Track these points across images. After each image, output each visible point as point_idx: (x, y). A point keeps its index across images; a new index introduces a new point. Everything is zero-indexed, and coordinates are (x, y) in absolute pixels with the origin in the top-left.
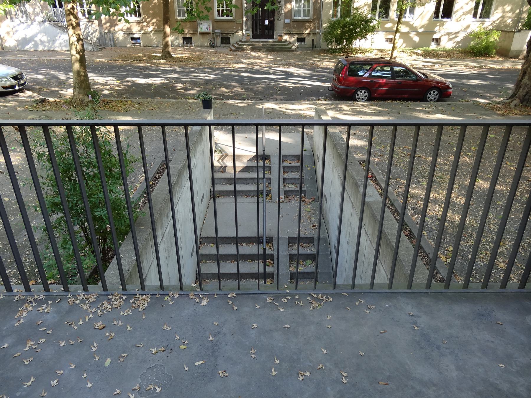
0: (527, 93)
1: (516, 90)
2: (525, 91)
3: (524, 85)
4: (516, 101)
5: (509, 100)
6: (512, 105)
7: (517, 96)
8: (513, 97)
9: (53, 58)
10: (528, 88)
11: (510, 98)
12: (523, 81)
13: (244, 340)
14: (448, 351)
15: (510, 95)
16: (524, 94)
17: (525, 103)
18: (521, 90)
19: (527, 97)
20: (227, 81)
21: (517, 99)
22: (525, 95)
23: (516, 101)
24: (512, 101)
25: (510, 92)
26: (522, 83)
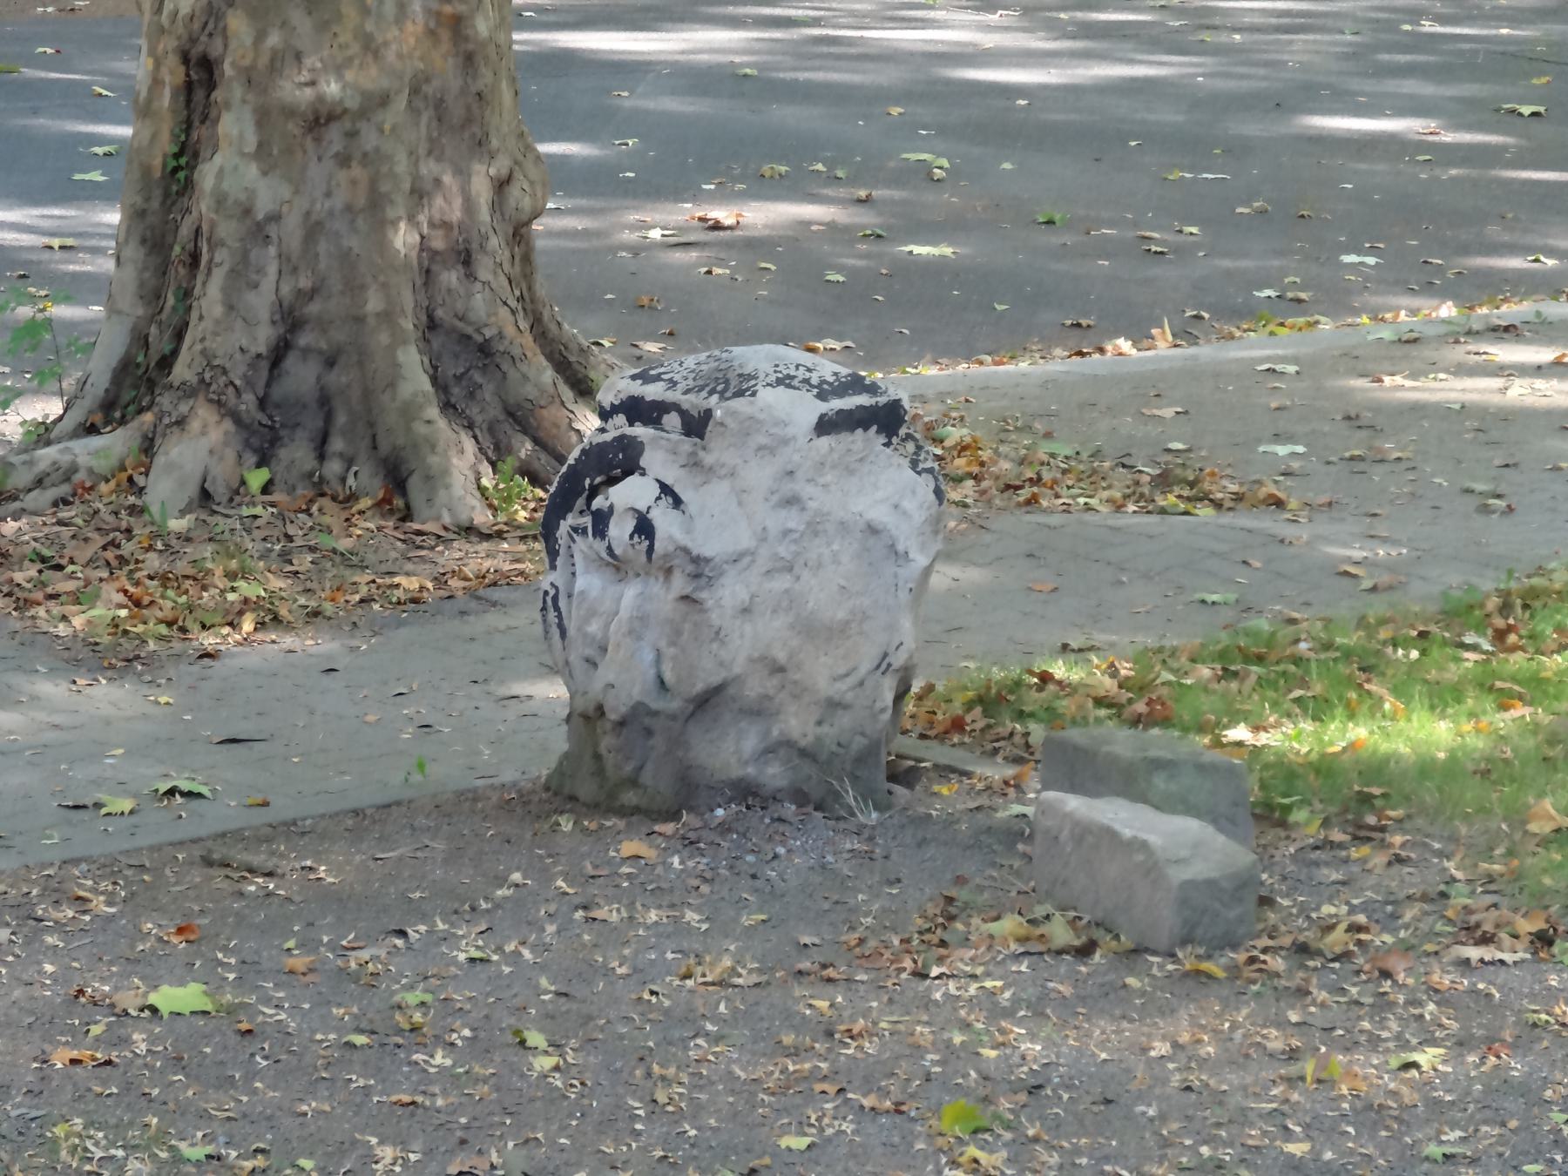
0: (290, 320)
1: (153, 297)
2: (261, 302)
3: (228, 230)
4: (199, 446)
5: (115, 444)
6: (165, 490)
7: (182, 371)
8: (135, 387)
9: (1059, 364)
10: (288, 267)
11: (110, 411)
12: (207, 176)
13: (863, 373)
14: (920, 921)
15: (99, 369)
16: (263, 338)
17: (297, 453)
18: (211, 296)
19: (301, 376)
20: (1500, 1084)
21: (203, 415)
22: (278, 354)
23: (199, 446)
24: (148, 447)
25: (95, 321)
26: (203, 206)
